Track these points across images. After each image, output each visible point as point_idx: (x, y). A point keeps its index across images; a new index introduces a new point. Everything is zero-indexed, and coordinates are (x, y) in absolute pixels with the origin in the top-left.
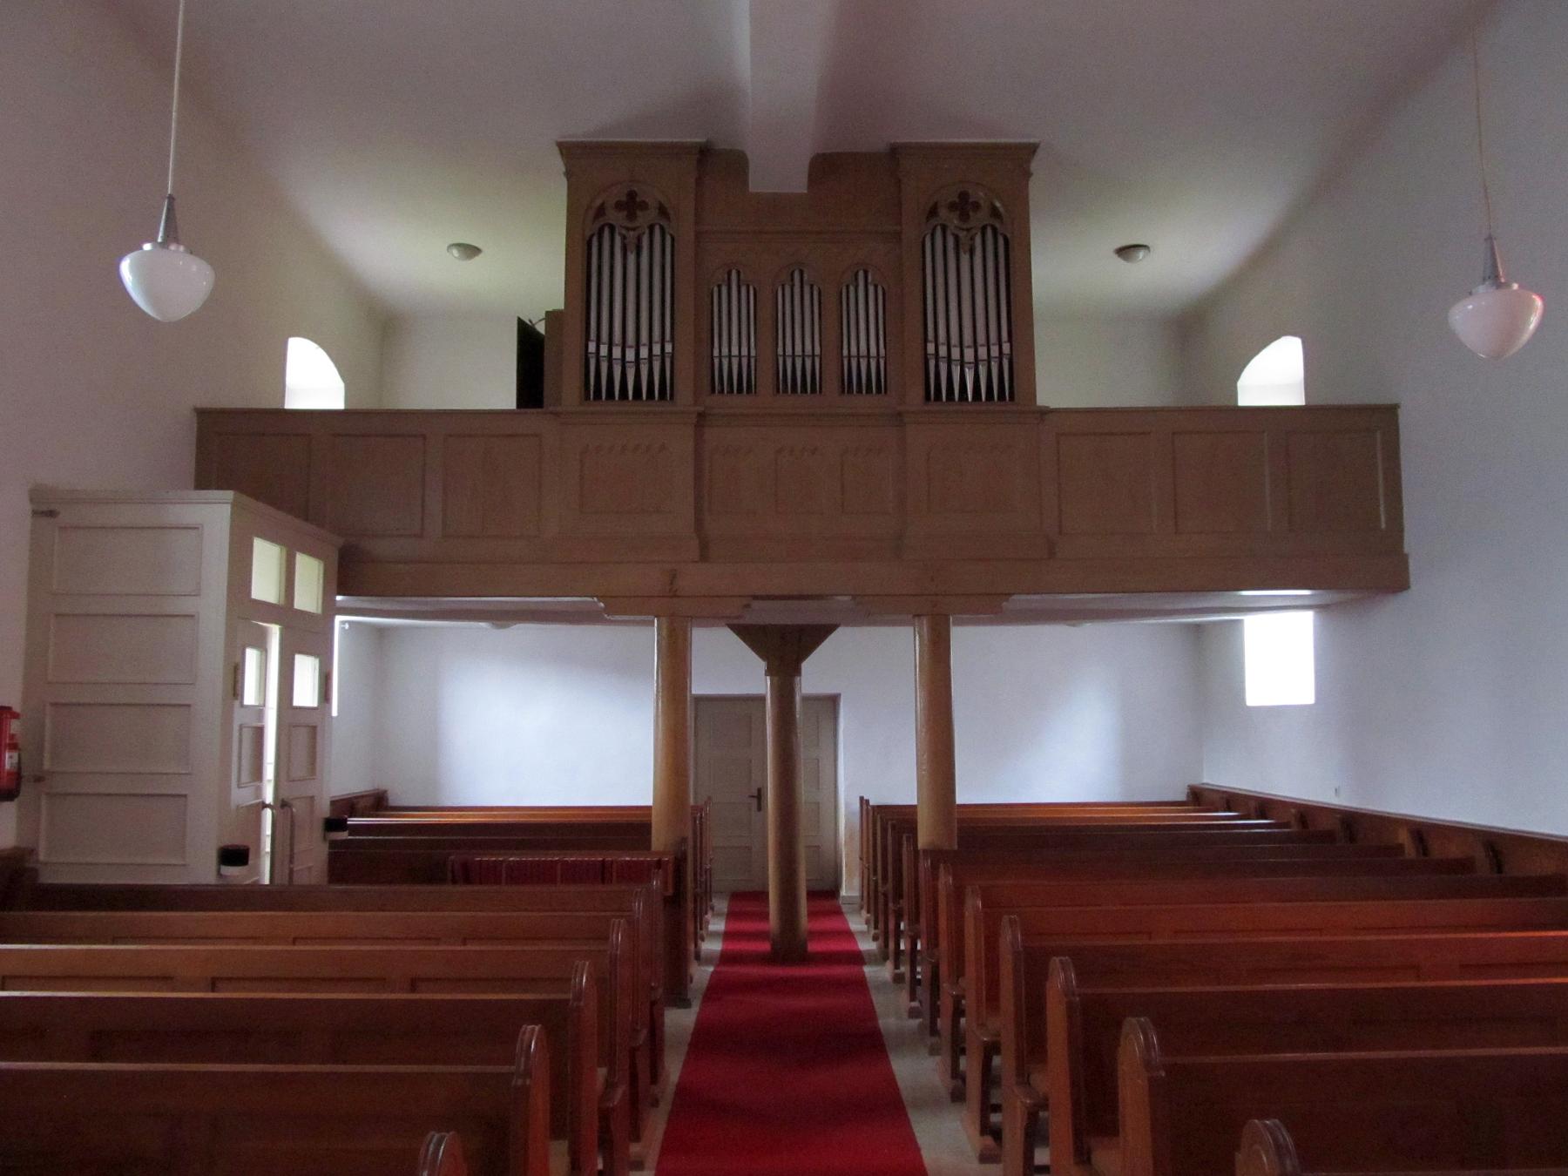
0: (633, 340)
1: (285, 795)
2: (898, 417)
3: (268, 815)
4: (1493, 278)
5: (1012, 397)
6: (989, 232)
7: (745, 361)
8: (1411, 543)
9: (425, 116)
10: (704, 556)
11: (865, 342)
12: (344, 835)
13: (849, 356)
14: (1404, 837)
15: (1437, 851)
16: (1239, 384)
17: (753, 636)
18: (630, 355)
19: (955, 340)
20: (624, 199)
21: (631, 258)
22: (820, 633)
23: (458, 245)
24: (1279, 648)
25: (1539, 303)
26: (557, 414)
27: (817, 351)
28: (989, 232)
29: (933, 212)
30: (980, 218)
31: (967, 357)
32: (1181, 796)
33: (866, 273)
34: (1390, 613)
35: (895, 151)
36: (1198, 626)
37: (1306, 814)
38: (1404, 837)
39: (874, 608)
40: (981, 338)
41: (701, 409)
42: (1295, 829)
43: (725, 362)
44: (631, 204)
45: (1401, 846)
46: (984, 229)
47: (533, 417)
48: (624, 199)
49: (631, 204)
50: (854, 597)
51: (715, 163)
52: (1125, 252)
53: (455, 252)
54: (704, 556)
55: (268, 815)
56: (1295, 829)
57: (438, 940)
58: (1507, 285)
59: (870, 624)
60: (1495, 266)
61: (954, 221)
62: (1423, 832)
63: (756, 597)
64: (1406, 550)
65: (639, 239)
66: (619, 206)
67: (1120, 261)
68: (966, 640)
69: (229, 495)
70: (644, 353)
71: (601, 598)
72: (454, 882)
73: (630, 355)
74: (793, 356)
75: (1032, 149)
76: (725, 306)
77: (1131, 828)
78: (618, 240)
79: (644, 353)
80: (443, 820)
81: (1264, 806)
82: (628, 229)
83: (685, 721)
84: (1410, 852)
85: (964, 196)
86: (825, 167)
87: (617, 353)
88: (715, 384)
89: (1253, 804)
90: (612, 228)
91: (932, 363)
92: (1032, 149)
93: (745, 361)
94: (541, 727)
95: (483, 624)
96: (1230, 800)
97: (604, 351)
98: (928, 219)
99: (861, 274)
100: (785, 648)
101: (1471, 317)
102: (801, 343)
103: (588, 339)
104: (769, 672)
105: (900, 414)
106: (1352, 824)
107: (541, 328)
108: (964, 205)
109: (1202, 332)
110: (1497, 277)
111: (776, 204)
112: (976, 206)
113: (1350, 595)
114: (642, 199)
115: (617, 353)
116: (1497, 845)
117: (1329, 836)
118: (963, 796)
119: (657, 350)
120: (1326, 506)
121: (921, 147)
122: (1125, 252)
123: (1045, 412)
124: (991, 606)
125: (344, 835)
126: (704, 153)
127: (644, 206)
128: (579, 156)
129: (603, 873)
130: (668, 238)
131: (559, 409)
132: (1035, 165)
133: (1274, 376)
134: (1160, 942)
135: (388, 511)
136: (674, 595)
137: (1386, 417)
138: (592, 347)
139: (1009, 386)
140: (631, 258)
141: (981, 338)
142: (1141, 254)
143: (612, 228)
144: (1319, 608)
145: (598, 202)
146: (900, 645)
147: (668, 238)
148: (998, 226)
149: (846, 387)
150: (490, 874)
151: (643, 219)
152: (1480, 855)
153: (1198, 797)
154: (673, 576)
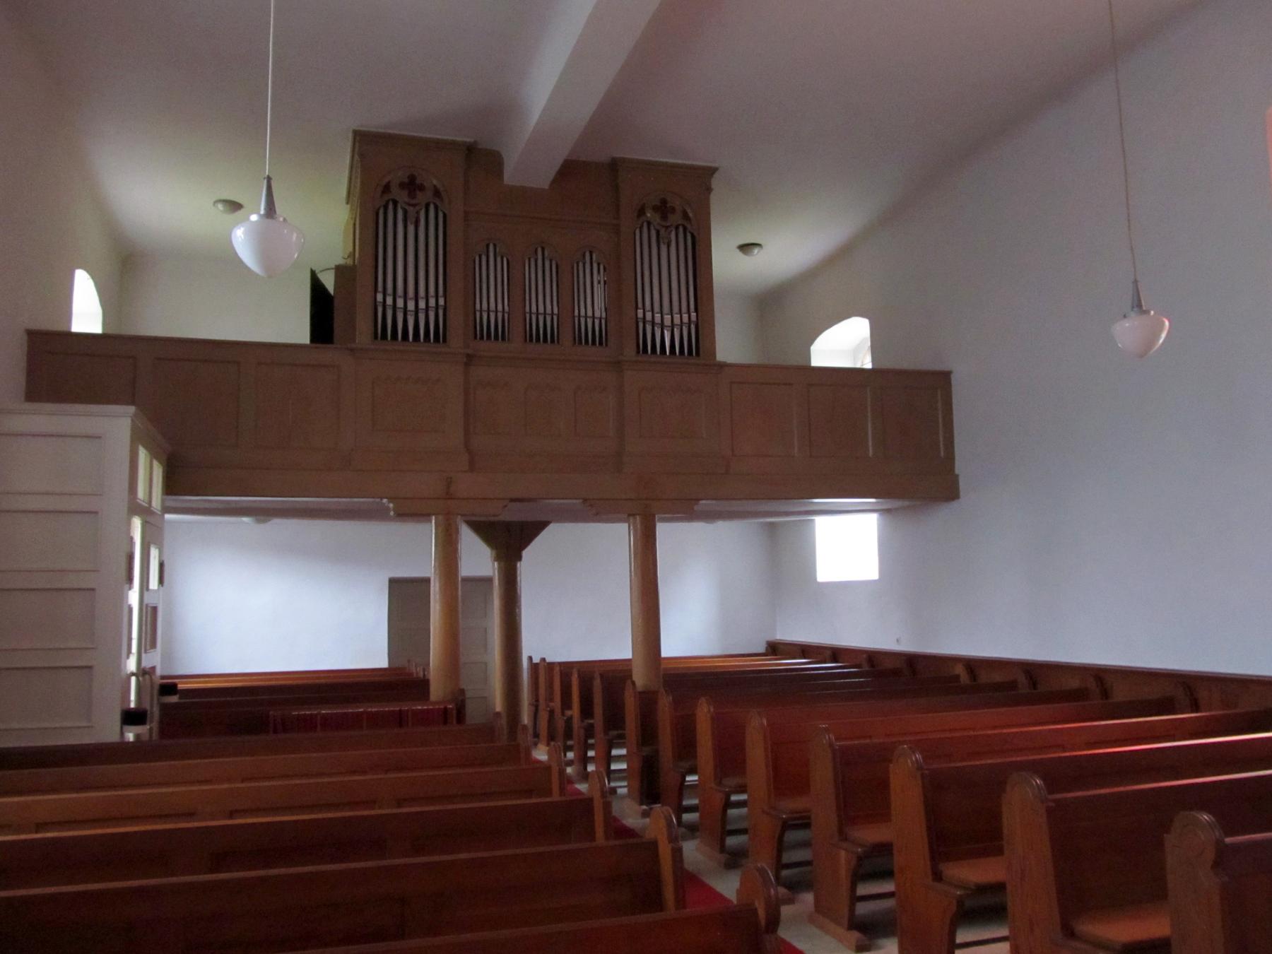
0: (412, 291)
1: (146, 664)
2: (617, 365)
3: (133, 679)
4: (1138, 306)
5: (698, 354)
6: (681, 229)
7: (500, 315)
8: (960, 467)
9: (213, 89)
10: (472, 468)
11: (594, 304)
12: (174, 699)
13: (531, 313)
14: (959, 670)
15: (984, 677)
16: (812, 348)
17: (486, 530)
18: (411, 306)
19: (657, 308)
20: (406, 180)
21: (411, 228)
22: (542, 525)
23: (226, 202)
24: (847, 543)
25: (1167, 323)
26: (352, 350)
27: (556, 311)
28: (681, 229)
29: (641, 212)
30: (675, 219)
31: (666, 318)
32: (762, 649)
33: (543, 249)
34: (944, 515)
35: (614, 165)
36: (772, 524)
37: (872, 657)
38: (959, 670)
39: (596, 509)
40: (676, 309)
41: (470, 351)
42: (866, 668)
43: (541, 318)
44: (412, 185)
45: (958, 677)
46: (677, 228)
47: (327, 354)
48: (406, 180)
49: (412, 185)
50: (585, 500)
51: (479, 159)
52: (746, 248)
53: (220, 206)
54: (472, 468)
55: (133, 679)
56: (866, 668)
57: (364, 773)
58: (1147, 312)
59: (599, 521)
60: (1140, 301)
61: (402, 196)
62: (973, 665)
63: (512, 500)
64: (957, 472)
65: (418, 213)
66: (655, 209)
67: (740, 254)
68: (666, 532)
69: (132, 409)
70: (422, 304)
71: (391, 499)
72: (275, 732)
73: (411, 306)
74: (538, 314)
75: (712, 171)
76: (675, 298)
77: (736, 673)
78: (653, 233)
79: (422, 304)
80: (210, 685)
81: (836, 654)
82: (409, 205)
83: (405, 597)
84: (965, 678)
85: (664, 202)
86: (570, 170)
87: (400, 303)
88: (479, 333)
89: (829, 653)
90: (395, 203)
91: (641, 325)
92: (712, 171)
93: (500, 315)
94: (265, 605)
95: (245, 519)
96: (804, 650)
97: (389, 301)
98: (383, 192)
99: (588, 255)
100: (510, 540)
101: (1127, 331)
102: (543, 305)
103: (376, 291)
104: (498, 558)
105: (619, 362)
106: (913, 662)
107: (329, 282)
108: (664, 209)
109: (789, 308)
110: (1140, 306)
111: (524, 195)
112: (673, 210)
113: (906, 503)
114: (416, 182)
115: (400, 303)
116: (1033, 671)
117: (895, 673)
118: (665, 653)
119: (432, 302)
120: (897, 441)
121: (631, 161)
122: (746, 248)
123: (723, 366)
124: (687, 509)
125: (174, 699)
126: (470, 150)
127: (422, 188)
128: (368, 144)
129: (400, 719)
130: (441, 215)
131: (353, 346)
132: (716, 182)
133: (844, 345)
134: (876, 741)
135: (223, 428)
136: (449, 496)
137: (941, 380)
138: (380, 297)
139: (697, 344)
140: (411, 228)
141: (676, 309)
142: (756, 250)
143: (395, 203)
144: (883, 512)
145: (386, 180)
146: (615, 538)
147: (441, 215)
148: (688, 226)
149: (578, 340)
150: (308, 724)
151: (421, 198)
152: (1022, 679)
153: (775, 649)
154: (449, 482)
